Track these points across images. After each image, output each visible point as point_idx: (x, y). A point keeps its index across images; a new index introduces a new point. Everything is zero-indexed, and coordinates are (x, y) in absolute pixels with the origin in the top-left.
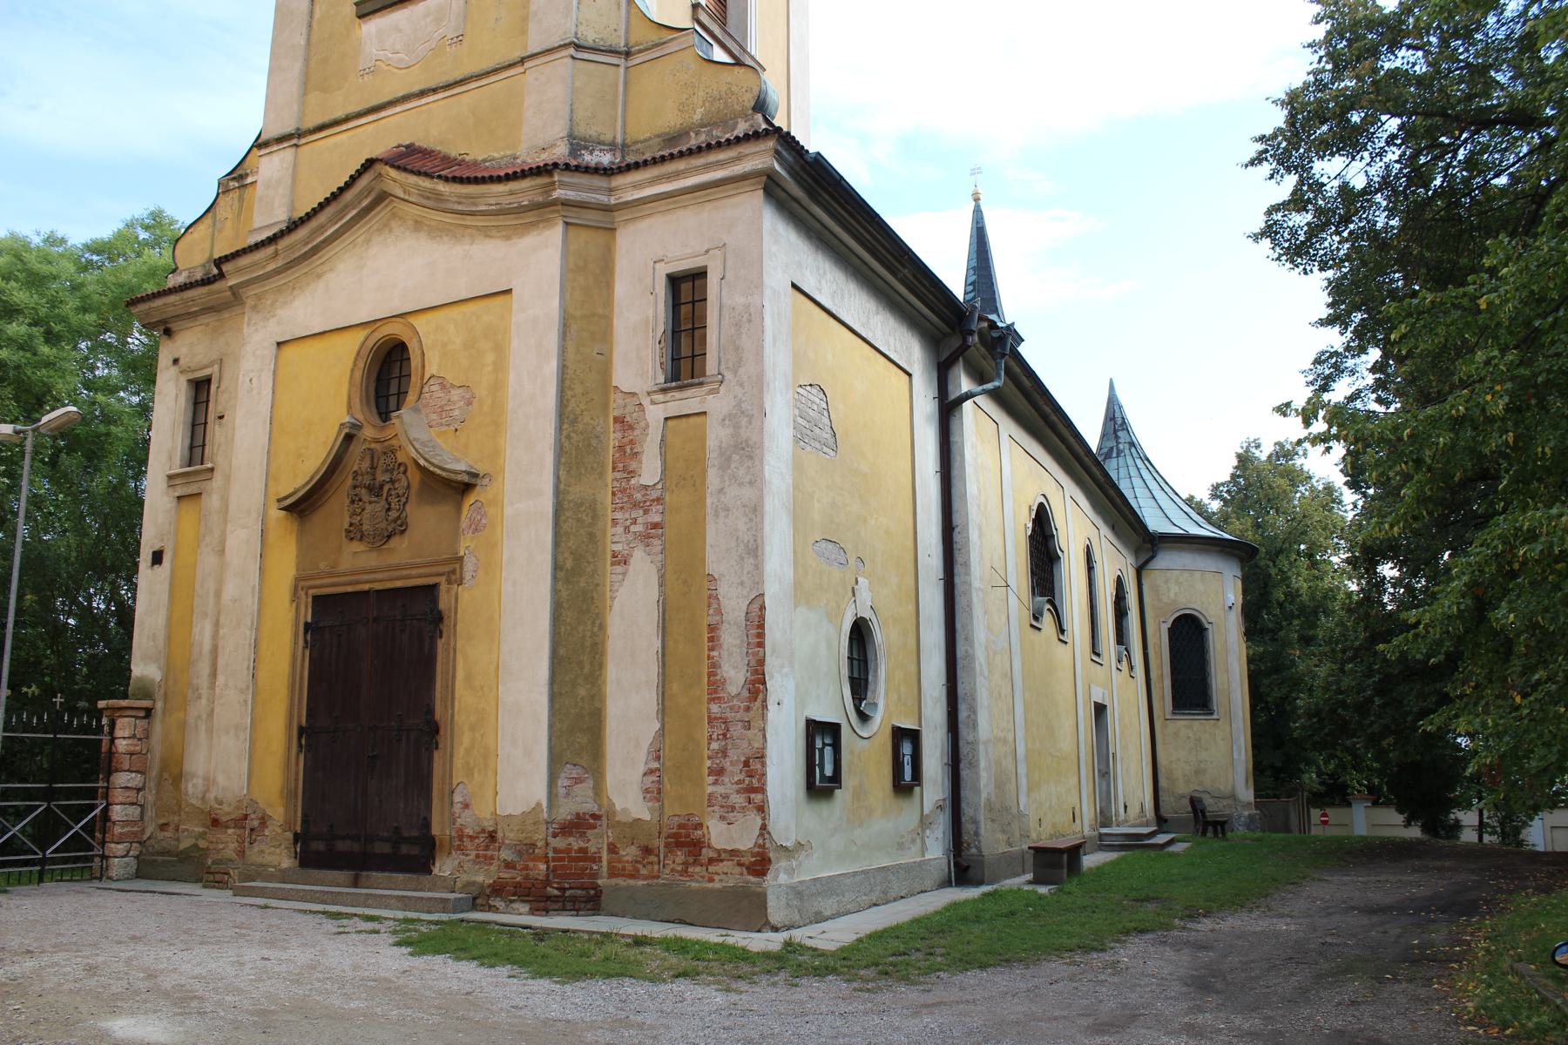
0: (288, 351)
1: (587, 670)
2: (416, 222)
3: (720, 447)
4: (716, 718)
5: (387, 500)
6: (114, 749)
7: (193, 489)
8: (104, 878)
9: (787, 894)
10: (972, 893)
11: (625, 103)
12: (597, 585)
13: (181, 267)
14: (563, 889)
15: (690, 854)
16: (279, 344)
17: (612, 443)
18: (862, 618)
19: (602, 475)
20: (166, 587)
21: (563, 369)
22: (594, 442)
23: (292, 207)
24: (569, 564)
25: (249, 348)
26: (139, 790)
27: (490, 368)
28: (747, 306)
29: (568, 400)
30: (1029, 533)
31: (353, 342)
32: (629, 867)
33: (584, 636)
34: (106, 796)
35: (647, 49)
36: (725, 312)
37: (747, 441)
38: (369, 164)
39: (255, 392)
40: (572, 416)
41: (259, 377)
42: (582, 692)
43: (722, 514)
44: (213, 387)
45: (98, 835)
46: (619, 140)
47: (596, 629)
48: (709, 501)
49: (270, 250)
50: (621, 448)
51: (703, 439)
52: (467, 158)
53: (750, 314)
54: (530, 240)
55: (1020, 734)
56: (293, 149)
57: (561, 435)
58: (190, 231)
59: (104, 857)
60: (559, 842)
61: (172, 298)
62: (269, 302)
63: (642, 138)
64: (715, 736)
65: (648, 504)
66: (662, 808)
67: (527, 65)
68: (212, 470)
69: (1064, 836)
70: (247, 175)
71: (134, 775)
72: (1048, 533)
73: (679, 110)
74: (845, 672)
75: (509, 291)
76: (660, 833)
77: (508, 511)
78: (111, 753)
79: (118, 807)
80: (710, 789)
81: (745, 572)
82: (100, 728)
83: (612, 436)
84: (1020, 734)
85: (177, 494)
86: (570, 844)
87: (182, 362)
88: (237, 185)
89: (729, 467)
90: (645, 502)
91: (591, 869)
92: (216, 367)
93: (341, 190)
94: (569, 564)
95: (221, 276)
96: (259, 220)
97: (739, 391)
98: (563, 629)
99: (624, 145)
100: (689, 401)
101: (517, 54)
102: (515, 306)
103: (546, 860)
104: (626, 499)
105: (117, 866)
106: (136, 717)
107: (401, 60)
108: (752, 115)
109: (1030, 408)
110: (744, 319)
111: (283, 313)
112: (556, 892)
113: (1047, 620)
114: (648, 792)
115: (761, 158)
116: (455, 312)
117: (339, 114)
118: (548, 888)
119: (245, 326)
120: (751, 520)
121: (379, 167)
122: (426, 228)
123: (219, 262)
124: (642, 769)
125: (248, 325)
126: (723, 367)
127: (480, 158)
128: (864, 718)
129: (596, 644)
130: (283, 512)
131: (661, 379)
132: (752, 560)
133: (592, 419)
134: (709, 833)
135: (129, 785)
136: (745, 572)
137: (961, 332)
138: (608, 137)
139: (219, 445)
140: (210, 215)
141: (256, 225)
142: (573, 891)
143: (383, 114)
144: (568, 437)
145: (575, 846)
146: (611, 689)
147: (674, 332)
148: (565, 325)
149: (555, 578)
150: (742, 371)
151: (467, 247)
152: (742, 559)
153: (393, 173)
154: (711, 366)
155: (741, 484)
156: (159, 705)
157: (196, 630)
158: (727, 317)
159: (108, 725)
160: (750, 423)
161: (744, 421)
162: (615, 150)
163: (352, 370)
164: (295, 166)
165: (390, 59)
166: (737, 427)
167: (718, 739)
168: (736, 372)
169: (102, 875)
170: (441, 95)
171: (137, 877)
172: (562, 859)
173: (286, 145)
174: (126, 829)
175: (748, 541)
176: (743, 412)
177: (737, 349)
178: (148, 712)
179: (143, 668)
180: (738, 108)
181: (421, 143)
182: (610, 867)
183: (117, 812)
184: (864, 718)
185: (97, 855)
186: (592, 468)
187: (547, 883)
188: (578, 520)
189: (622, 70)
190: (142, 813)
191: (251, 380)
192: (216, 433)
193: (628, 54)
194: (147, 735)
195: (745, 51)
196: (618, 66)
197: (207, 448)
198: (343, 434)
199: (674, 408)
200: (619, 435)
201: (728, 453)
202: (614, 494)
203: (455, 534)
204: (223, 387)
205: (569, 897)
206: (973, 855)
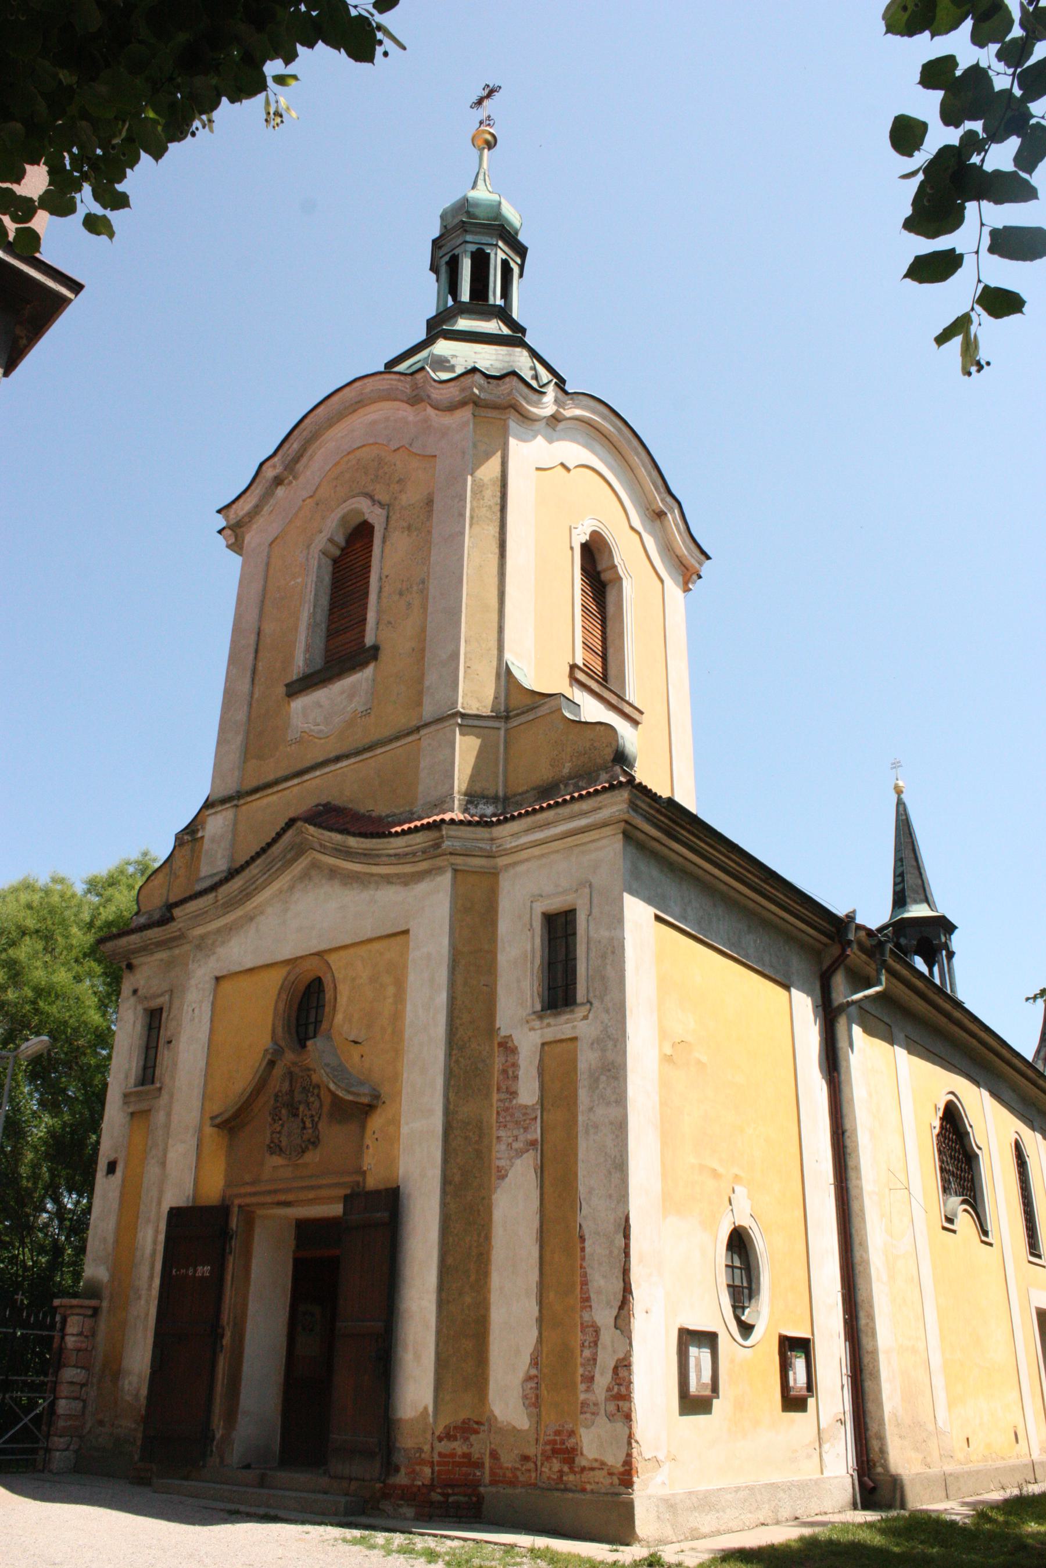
0: (226, 986)
1: (473, 1278)
2: (331, 870)
3: (590, 1068)
4: (587, 1327)
5: (302, 1119)
6: (63, 1345)
7: (143, 1106)
8: (46, 1471)
9: (658, 1506)
10: (871, 1516)
11: (506, 760)
12: (483, 1198)
13: (143, 910)
14: (446, 1495)
15: (565, 1461)
16: (218, 979)
17: (496, 1067)
18: (740, 1226)
19: (488, 1096)
20: (117, 1194)
21: (452, 1000)
22: (480, 1066)
23: (232, 859)
24: (457, 1178)
25: (193, 982)
26: (82, 1385)
27: (390, 1000)
28: (612, 939)
29: (457, 1028)
30: (937, 1131)
31: (276, 977)
32: (509, 1474)
33: (470, 1248)
34: (54, 1390)
35: (523, 713)
36: (592, 945)
37: (613, 1063)
38: (291, 823)
39: (196, 1020)
40: (460, 1043)
41: (200, 1007)
42: (468, 1300)
43: (592, 1131)
44: (164, 1015)
45: (44, 1428)
46: (501, 794)
47: (481, 1240)
48: (580, 1118)
49: (211, 897)
50: (505, 1072)
51: (574, 1061)
52: (374, 814)
53: (614, 947)
54: (422, 887)
55: (934, 1341)
56: (234, 810)
57: (450, 1060)
58: (152, 878)
59: (48, 1450)
60: (445, 1447)
61: (133, 938)
62: (210, 942)
63: (520, 791)
64: (586, 1344)
65: (528, 1122)
66: (539, 1415)
67: (423, 732)
68: (160, 1089)
69: (1003, 1458)
70: (198, 830)
71: (79, 1370)
72: (962, 1131)
73: (551, 765)
74: (723, 1280)
75: (406, 932)
76: (537, 1440)
77: (404, 1130)
78: (61, 1349)
79: (63, 1400)
80: (582, 1397)
81: (613, 1186)
82: (52, 1327)
83: (497, 1060)
84: (934, 1341)
85: (130, 1110)
86: (454, 1449)
87: (140, 993)
88: (190, 838)
89: (597, 1087)
90: (525, 1120)
91: (475, 1475)
92: (167, 997)
93: (269, 845)
94: (457, 1178)
95: (172, 919)
96: (205, 870)
97: (605, 1017)
98: (451, 1239)
99: (506, 798)
100: (562, 1026)
101: (414, 723)
102: (412, 945)
103: (432, 1464)
104: (508, 1119)
105: (59, 1459)
106: (85, 1316)
107: (321, 731)
108: (612, 767)
109: (930, 1008)
110: (609, 951)
111: (221, 951)
112: (440, 1498)
113: (965, 1222)
114: (527, 1398)
115: (616, 805)
116: (362, 951)
117: (271, 777)
118: (432, 1494)
119: (190, 962)
120: (617, 1136)
121: (299, 824)
122: (338, 876)
123: (171, 907)
124: (521, 1375)
125: (193, 961)
126: (591, 995)
127: (384, 814)
128: (746, 1329)
129: (481, 1254)
130: (215, 1129)
131: (538, 1007)
132: (618, 1175)
133: (479, 1045)
134: (581, 1441)
135: (74, 1380)
136: (613, 1186)
137: (840, 942)
138: (491, 792)
139: (167, 1068)
140: (167, 865)
141: (203, 874)
142: (456, 1497)
143: (306, 777)
144: (457, 1062)
145: (459, 1451)
146: (495, 1298)
147: (550, 964)
148: (454, 961)
149: (444, 1192)
150: (607, 998)
151: (372, 892)
152: (610, 1173)
153: (311, 829)
154: (581, 995)
155: (608, 1104)
156: (105, 1304)
157: (140, 1235)
158: (594, 950)
159: (61, 1323)
160: (615, 1046)
161: (610, 1044)
162: (497, 803)
163: (277, 1002)
164: (235, 823)
165: (311, 730)
166: (604, 1050)
167: (590, 1347)
168: (602, 1001)
169: (44, 1467)
170: (353, 760)
171: (75, 1471)
172: (446, 1464)
173: (228, 805)
174: (69, 1423)
175: (615, 1157)
176: (609, 1037)
177: (603, 978)
178: (96, 1311)
179: (95, 1270)
180: (599, 761)
181: (338, 802)
182: (492, 1473)
183: (63, 1406)
184: (746, 1329)
185: (41, 1448)
186: (479, 1090)
187: (432, 1487)
188: (466, 1138)
189: (502, 732)
190: (84, 1407)
191: (193, 1010)
192: (165, 1056)
193: (507, 718)
194: (93, 1333)
195: (623, 699)
196: (499, 729)
197: (157, 1069)
198: (266, 1060)
199: (550, 1034)
200: (503, 1059)
201: (597, 1074)
202: (498, 1113)
203: (360, 1149)
204: (171, 1016)
205: (453, 1502)
206: (879, 1474)
